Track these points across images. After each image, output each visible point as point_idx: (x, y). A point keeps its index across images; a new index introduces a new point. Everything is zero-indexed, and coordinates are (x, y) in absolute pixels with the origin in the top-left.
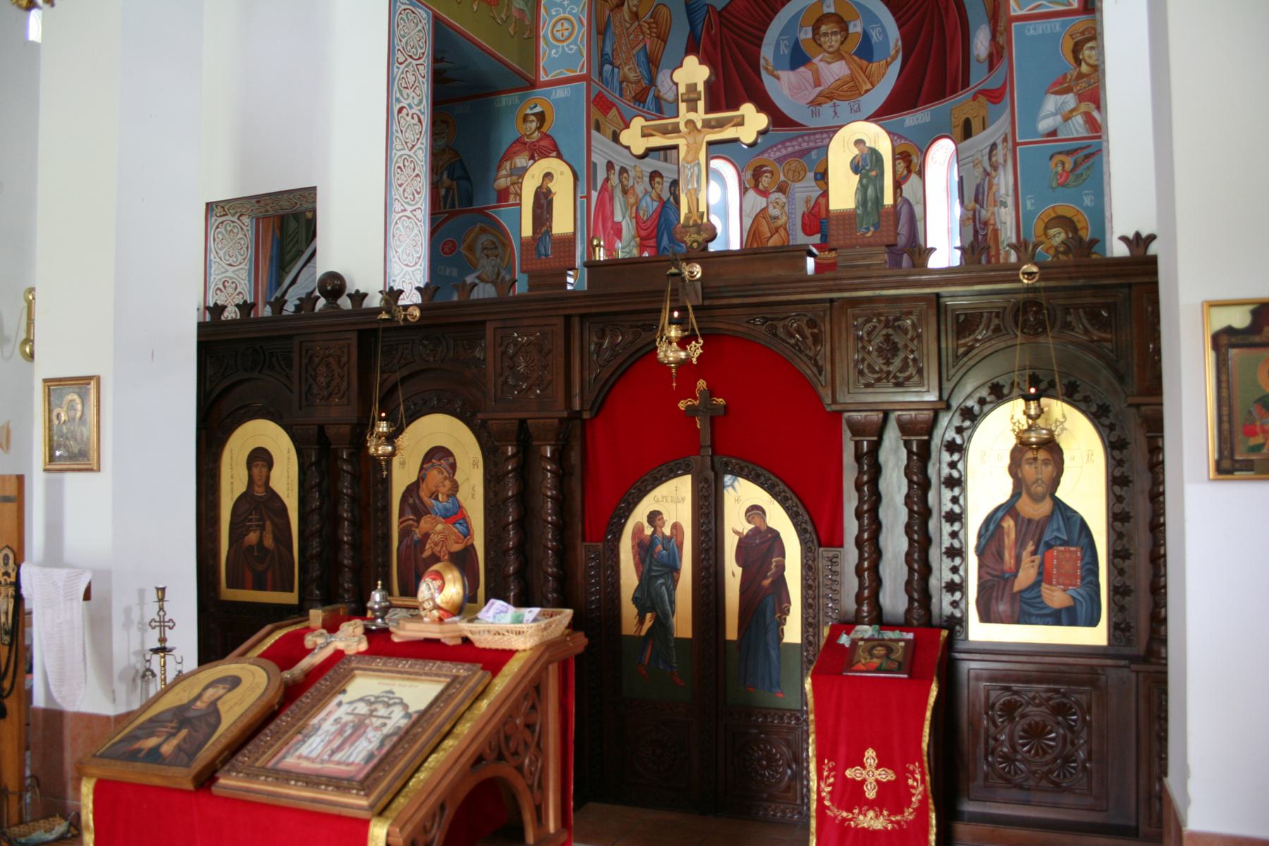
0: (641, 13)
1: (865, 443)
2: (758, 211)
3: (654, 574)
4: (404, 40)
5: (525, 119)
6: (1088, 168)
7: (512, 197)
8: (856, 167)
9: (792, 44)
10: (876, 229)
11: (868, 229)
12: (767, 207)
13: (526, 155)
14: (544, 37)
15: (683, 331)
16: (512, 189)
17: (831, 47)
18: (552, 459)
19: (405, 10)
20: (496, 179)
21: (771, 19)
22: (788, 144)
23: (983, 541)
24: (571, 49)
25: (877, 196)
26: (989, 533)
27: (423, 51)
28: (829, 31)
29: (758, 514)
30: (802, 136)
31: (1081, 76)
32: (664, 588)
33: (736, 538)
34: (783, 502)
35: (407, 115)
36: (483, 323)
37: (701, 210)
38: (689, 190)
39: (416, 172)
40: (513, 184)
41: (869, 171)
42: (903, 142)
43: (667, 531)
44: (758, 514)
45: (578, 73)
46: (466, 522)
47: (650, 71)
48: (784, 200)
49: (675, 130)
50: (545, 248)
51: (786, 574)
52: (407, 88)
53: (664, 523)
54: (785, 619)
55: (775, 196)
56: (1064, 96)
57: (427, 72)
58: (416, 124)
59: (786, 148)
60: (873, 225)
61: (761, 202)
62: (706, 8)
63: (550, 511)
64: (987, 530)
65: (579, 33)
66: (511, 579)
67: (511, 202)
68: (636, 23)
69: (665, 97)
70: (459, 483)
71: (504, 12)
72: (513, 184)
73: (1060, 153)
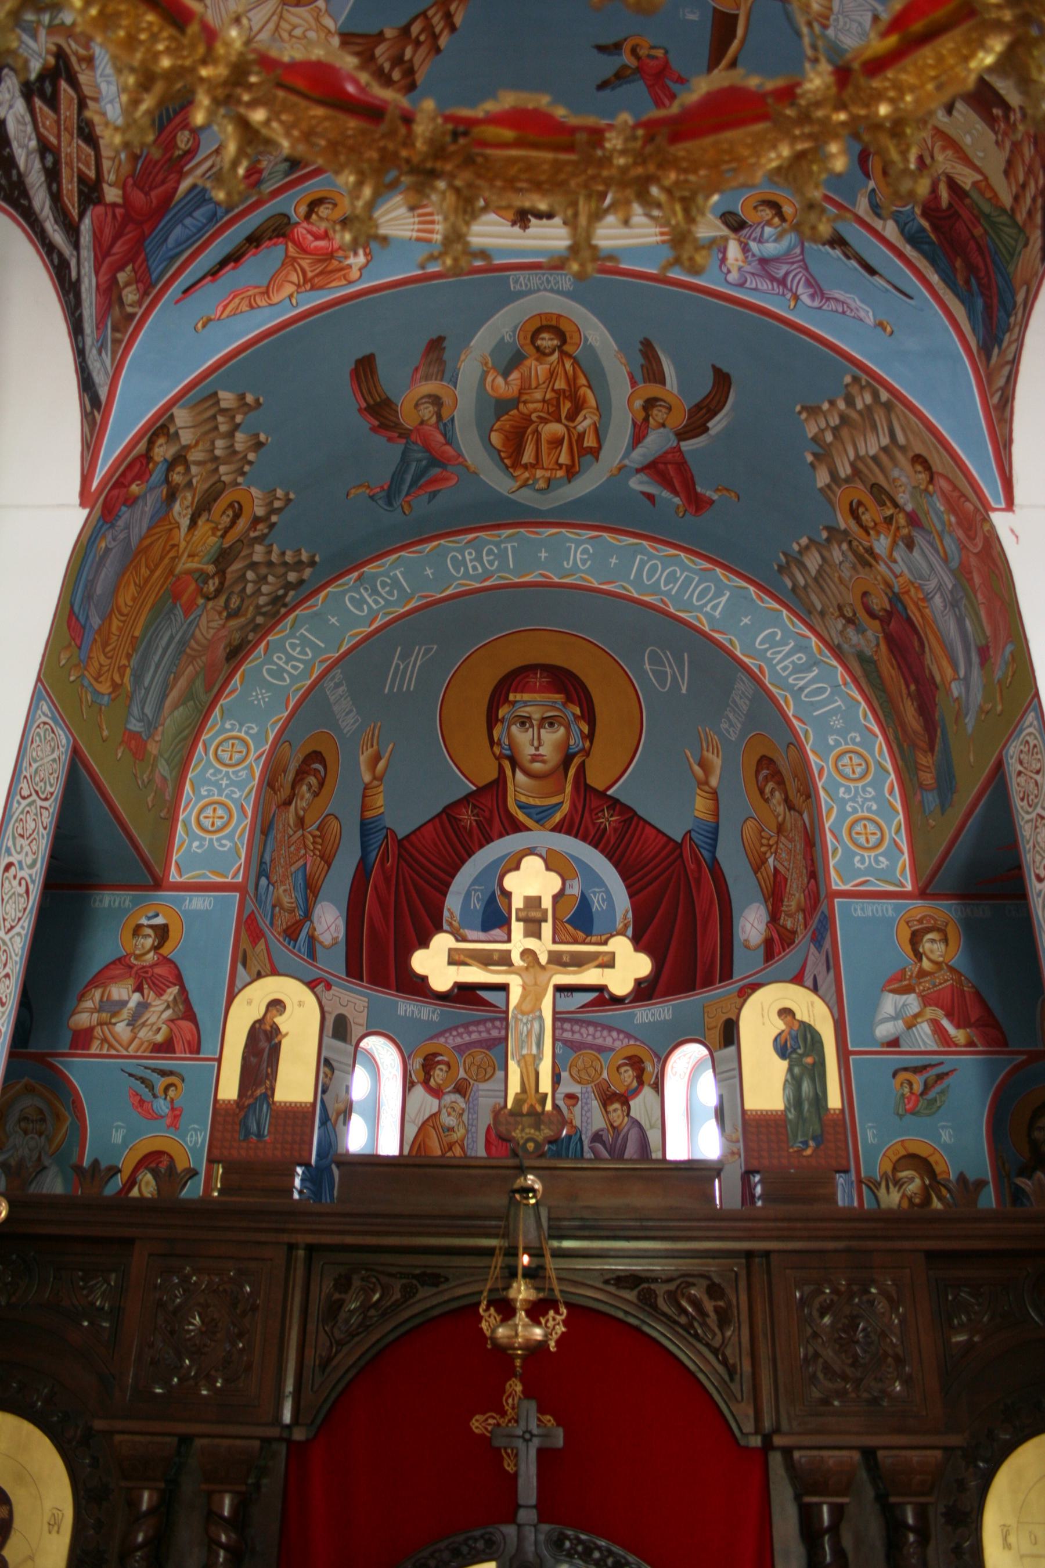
0: (307, 821)
2: (427, 1116)
4: (35, 766)
5: (137, 930)
7: (96, 1043)
8: (782, 1049)
9: (486, 898)
11: (806, 1143)
12: (439, 1112)
13: (130, 983)
14: (184, 821)
15: (538, 1289)
16: (98, 1031)
19: (45, 723)
20: (73, 1013)
21: (463, 862)
22: (472, 1028)
24: (224, 846)
25: (816, 1094)
27: (52, 790)
30: (492, 1020)
31: (922, 974)
35: (15, 877)
37: (542, 1090)
38: (524, 1056)
39: (7, 970)
40: (101, 1024)
41: (802, 1056)
45: (229, 880)
48: (463, 1105)
49: (504, 960)
52: (22, 836)
55: (449, 1098)
56: (905, 997)
57: (51, 822)
58: (20, 895)
59: (470, 1033)
60: (814, 1138)
61: (432, 1104)
62: (385, 831)
68: (300, 832)
69: (322, 938)
71: (147, 773)
72: (101, 1024)
73: (906, 1069)
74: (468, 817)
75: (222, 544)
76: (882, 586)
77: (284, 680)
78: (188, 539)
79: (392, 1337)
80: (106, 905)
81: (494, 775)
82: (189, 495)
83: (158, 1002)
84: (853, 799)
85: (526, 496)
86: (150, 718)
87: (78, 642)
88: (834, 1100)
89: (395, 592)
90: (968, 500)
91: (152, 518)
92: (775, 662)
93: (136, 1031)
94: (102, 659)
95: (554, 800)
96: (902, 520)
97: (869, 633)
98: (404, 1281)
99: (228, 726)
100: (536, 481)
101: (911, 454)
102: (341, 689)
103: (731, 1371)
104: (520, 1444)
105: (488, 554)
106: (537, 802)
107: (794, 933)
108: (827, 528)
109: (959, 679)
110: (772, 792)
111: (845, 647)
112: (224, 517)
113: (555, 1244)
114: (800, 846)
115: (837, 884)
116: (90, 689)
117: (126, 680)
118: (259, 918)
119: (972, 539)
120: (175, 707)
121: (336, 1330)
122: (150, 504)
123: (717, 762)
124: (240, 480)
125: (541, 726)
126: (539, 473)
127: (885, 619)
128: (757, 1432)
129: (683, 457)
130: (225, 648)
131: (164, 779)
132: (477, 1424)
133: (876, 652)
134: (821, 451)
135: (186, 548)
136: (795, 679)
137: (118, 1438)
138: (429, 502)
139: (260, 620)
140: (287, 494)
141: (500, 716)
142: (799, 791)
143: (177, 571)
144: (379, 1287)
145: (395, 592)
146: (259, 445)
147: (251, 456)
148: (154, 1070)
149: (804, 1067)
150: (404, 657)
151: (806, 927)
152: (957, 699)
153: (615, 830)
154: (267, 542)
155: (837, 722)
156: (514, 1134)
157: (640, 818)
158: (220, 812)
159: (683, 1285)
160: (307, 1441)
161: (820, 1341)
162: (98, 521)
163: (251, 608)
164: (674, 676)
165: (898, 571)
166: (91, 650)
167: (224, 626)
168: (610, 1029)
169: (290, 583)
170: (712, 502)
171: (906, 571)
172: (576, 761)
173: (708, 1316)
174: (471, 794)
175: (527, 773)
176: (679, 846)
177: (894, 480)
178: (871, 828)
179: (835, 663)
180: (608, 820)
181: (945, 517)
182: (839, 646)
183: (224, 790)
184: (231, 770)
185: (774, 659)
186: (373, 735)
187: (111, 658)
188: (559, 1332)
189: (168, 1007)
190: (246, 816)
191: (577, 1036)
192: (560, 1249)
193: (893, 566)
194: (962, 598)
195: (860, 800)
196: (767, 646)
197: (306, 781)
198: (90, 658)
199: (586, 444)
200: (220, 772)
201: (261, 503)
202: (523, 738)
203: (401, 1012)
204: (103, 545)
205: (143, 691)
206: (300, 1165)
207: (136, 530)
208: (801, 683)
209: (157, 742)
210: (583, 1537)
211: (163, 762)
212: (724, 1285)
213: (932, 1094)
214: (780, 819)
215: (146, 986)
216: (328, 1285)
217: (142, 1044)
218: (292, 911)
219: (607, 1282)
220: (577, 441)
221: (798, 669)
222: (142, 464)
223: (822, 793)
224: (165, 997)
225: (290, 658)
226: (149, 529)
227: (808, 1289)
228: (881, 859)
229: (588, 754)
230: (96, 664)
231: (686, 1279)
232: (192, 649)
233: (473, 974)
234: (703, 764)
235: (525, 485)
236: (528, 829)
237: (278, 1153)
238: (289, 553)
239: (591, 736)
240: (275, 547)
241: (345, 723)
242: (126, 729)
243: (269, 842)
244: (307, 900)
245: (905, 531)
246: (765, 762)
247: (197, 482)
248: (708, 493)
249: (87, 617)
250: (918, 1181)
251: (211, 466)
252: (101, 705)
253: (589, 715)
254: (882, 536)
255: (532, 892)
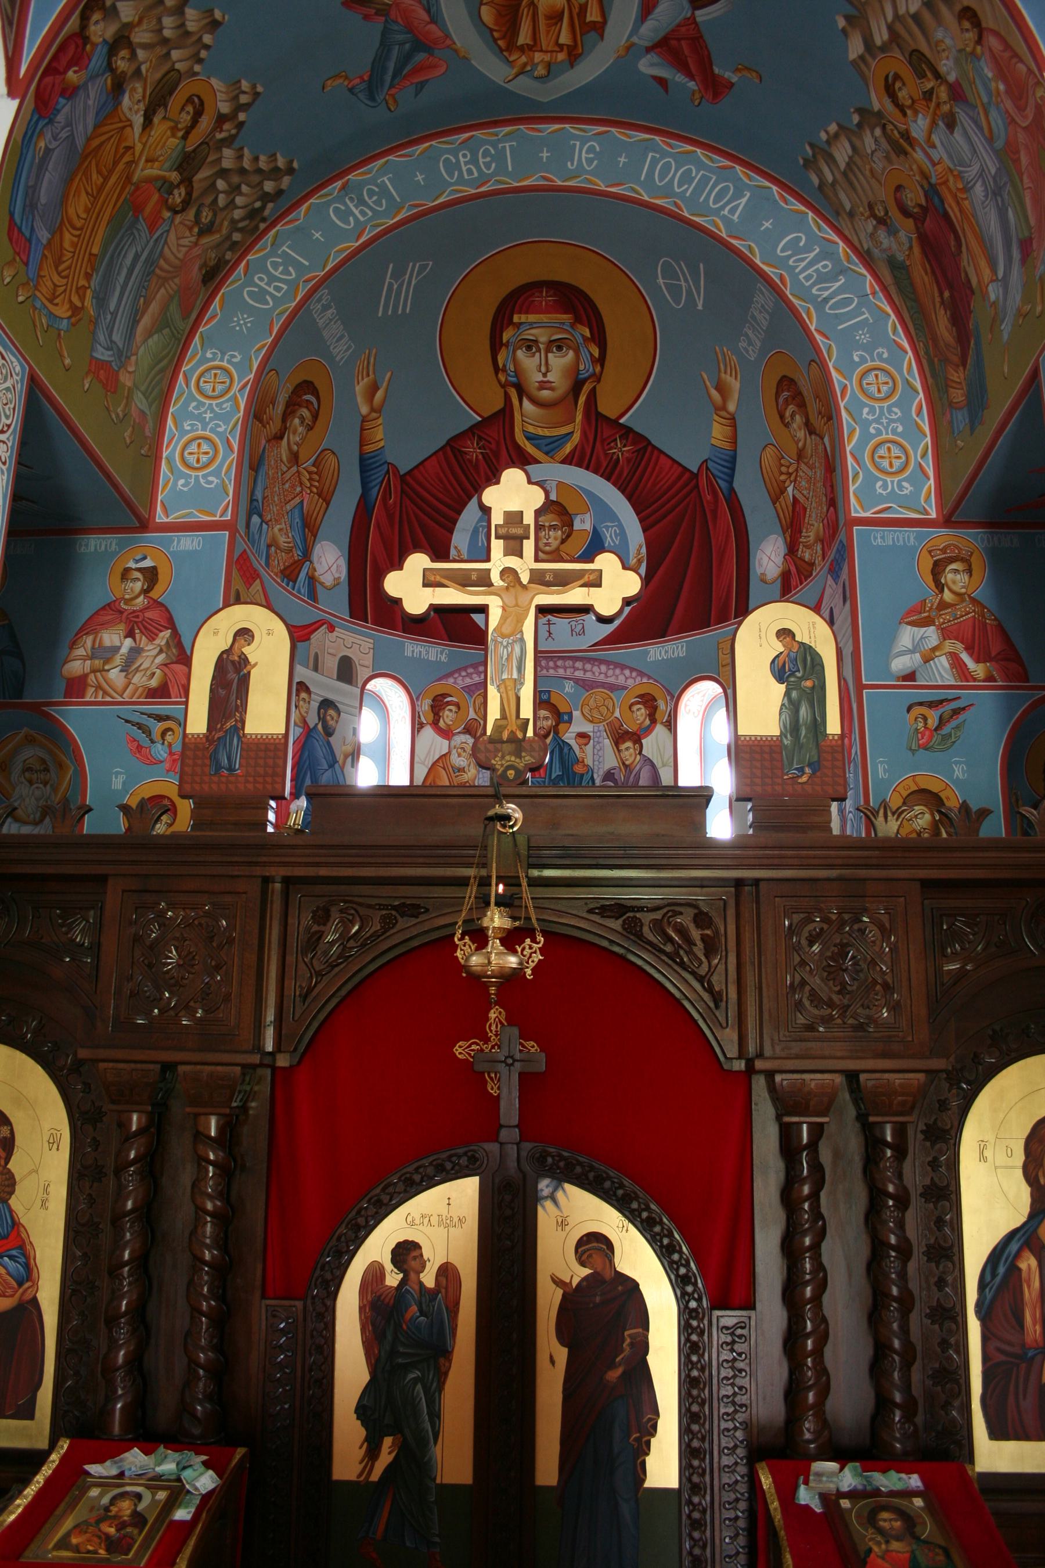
0: (302, 457)
1: (805, 1127)
2: (437, 757)
3: (400, 1360)
5: (125, 574)
6: (957, 727)
7: (91, 691)
8: (780, 671)
10: (814, 773)
11: (801, 770)
12: (449, 753)
15: (514, 918)
17: (547, 544)
18: (218, 1142)
20: (66, 662)
23: (989, 1294)
24: (211, 482)
26: (998, 1279)
27: (8, 422)
28: (547, 524)
29: (600, 1249)
31: (943, 605)
32: (419, 1387)
33: (560, 1292)
34: (647, 1227)
36: (103, 879)
38: (503, 680)
40: (94, 671)
41: (801, 679)
42: (645, 680)
43: (429, 1278)
44: (600, 1249)
45: (217, 518)
46: (27, 1257)
47: (305, 540)
49: (483, 580)
50: (229, 759)
51: (651, 1359)
53: (424, 1267)
54: (648, 1444)
57: (10, 457)
60: (810, 765)
61: (441, 745)
62: (386, 466)
63: (208, 1241)
64: (994, 1275)
65: (224, 459)
66: (119, 1375)
67: (87, 699)
69: (322, 579)
70: (17, 1178)
71: (122, 406)
72: (94, 671)
73: (921, 704)
74: (473, 450)
75: (184, 147)
76: (918, 178)
77: (268, 303)
78: (144, 140)
79: (372, 968)
80: (93, 549)
81: (499, 405)
82: (139, 86)
83: (150, 647)
84: (877, 421)
85: (524, 86)
86: (121, 346)
87: (25, 258)
88: (833, 726)
89: (384, 201)
90: (1021, 61)
91: (97, 114)
92: (797, 271)
93: (130, 676)
94: (56, 279)
95: (564, 430)
96: (943, 93)
97: (902, 234)
98: (384, 912)
99: (209, 355)
100: (535, 66)
101: (958, 8)
102: (330, 311)
103: (717, 998)
104: (502, 1067)
105: (484, 156)
106: (546, 432)
107: (812, 564)
108: (860, 111)
109: (997, 280)
110: (792, 416)
111: (876, 252)
112: (184, 115)
113: (535, 873)
114: (820, 473)
115: (856, 511)
116: (45, 312)
117: (88, 302)
118: (252, 557)
119: (1021, 109)
120: (149, 334)
121: (315, 962)
122: (94, 95)
123: (735, 385)
124: (197, 68)
125: (548, 350)
126: (538, 57)
127: (919, 216)
128: (740, 1057)
129: (699, 29)
130: (200, 269)
131: (143, 412)
132: (460, 1050)
133: (908, 255)
134: (853, 12)
135: (143, 150)
136: (819, 290)
137: (102, 1066)
138: (416, 95)
139: (237, 237)
140: (254, 87)
141: (504, 341)
142: (820, 413)
143: (135, 179)
144: (358, 919)
145: (384, 201)
146: (214, 25)
147: (207, 39)
148: (150, 716)
149: (802, 691)
150: (397, 275)
151: (824, 558)
152: (994, 303)
153: (629, 460)
154: (236, 145)
155: (863, 337)
156: (493, 762)
157: (655, 447)
158: (205, 447)
159: (670, 914)
160: (291, 1066)
161: (808, 968)
162: (32, 115)
163: (226, 223)
164: (689, 292)
165: (936, 157)
166: (40, 268)
167: (196, 244)
168: (623, 667)
169: (267, 194)
170: (732, 85)
171: (945, 157)
172: (587, 388)
173: (695, 945)
174: (477, 426)
175: (534, 401)
176: (695, 476)
177: (939, 42)
178: (896, 451)
179: (864, 271)
180: (621, 450)
181: (993, 85)
182: (868, 252)
183: (208, 423)
184: (214, 402)
185: (797, 267)
186: (368, 363)
187: (67, 277)
188: (536, 960)
189: (161, 651)
190: (232, 451)
191: (589, 675)
192: (540, 878)
193: (930, 151)
194: (1005, 184)
195: (884, 421)
196: (790, 252)
197: (298, 414)
198: (40, 276)
199: (589, 19)
200: (204, 404)
201: (224, 97)
202: (529, 363)
203: (408, 653)
204: (42, 144)
205: (109, 317)
206: (273, 798)
207: (81, 128)
208: (826, 294)
209: (130, 373)
210: (566, 1154)
211: (140, 395)
212: (712, 913)
213: (946, 730)
214: (800, 444)
215: (137, 631)
216: (307, 919)
217: (137, 689)
218: (289, 551)
219: (591, 911)
220: (579, 15)
221: (823, 278)
222: (77, 46)
223: (844, 414)
224: (157, 642)
225: (272, 279)
226: (96, 127)
227: (796, 918)
228: (905, 484)
229: (599, 381)
230: (49, 284)
231: (673, 907)
232: (161, 269)
233: (451, 596)
234: (720, 387)
235: (521, 72)
236: (538, 462)
237: (250, 786)
238: (263, 158)
239: (601, 360)
240: (246, 151)
241: (337, 350)
242: (92, 357)
243: (260, 478)
244: (305, 540)
245: (946, 108)
246: (786, 383)
247: (147, 71)
248: (727, 75)
249: (32, 229)
250: (927, 817)
251: (161, 51)
252: (59, 330)
253: (599, 337)
254: (920, 115)
255: (514, 508)
